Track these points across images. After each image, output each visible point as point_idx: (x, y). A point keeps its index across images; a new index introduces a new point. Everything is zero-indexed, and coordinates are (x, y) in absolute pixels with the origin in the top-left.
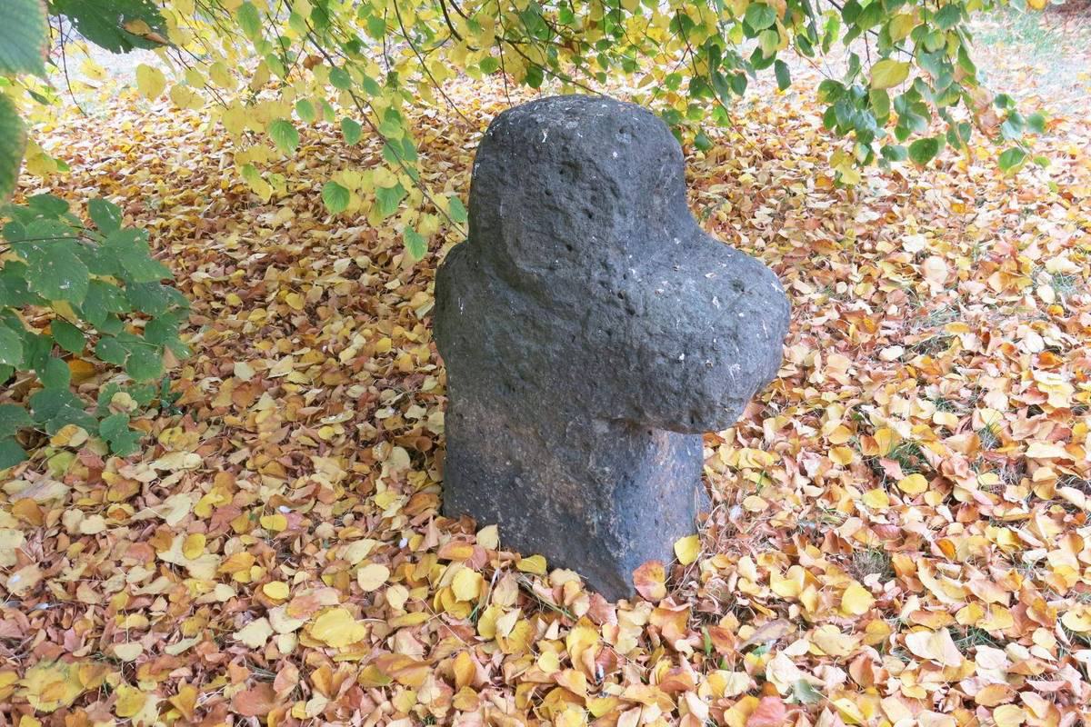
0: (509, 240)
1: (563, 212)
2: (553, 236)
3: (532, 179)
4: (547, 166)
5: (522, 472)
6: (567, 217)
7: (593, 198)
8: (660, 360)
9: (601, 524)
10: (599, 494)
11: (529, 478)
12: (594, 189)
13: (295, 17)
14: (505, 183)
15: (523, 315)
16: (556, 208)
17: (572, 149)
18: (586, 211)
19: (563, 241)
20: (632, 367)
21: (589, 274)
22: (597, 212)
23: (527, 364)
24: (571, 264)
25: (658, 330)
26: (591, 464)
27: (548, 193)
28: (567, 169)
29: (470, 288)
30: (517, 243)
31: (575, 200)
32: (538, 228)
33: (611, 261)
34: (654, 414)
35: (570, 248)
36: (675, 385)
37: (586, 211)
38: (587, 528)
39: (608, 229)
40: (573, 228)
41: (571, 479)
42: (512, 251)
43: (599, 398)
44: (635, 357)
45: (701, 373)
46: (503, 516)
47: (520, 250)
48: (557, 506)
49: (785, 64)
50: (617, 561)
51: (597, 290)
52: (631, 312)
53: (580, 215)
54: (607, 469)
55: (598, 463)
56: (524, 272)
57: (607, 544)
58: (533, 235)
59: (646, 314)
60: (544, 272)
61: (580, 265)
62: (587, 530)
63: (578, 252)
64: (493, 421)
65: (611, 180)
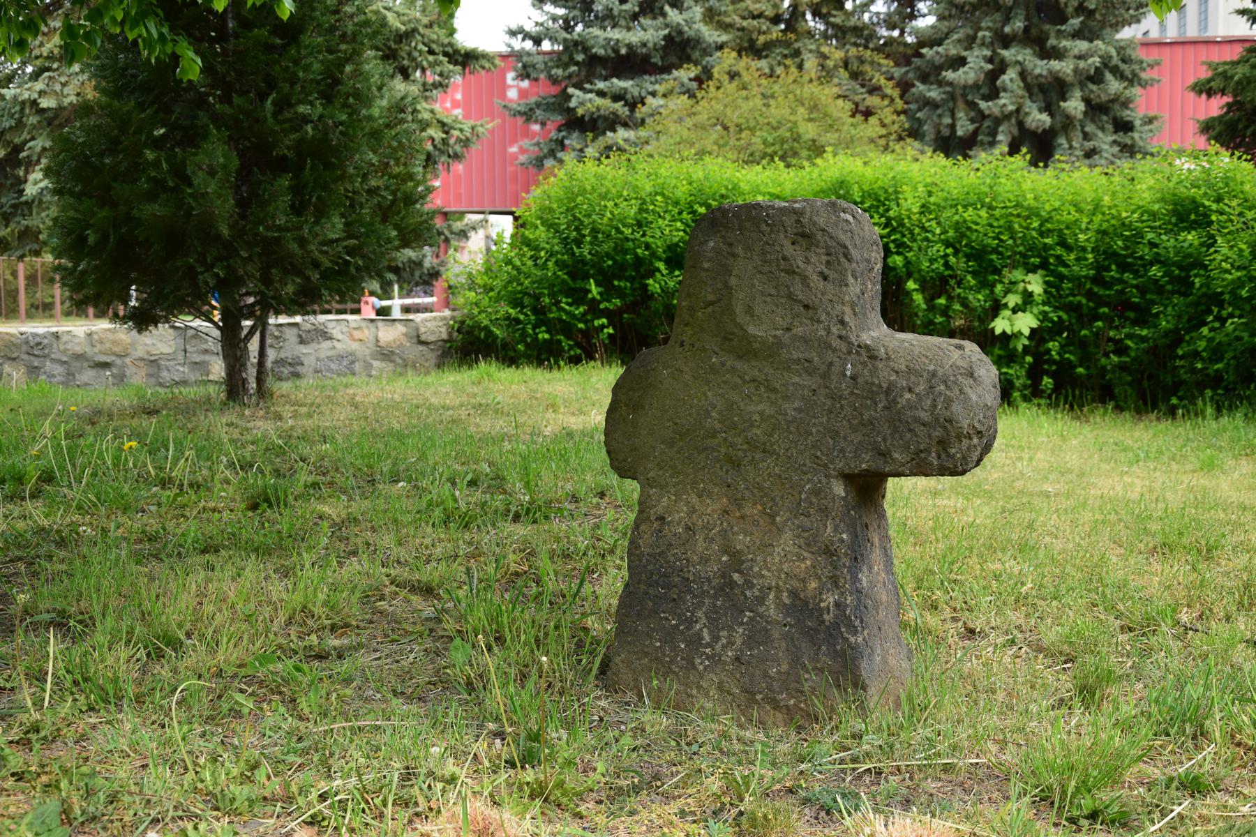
0: (739, 309)
1: (800, 275)
2: (790, 297)
3: (768, 248)
4: (782, 236)
5: (742, 562)
6: (804, 278)
7: (828, 263)
8: (907, 396)
9: (837, 604)
10: (835, 568)
11: (751, 568)
12: (828, 254)
13: (101, 352)
14: (734, 255)
15: (754, 381)
16: (794, 272)
17: (805, 220)
18: (821, 274)
19: (800, 301)
20: (880, 406)
21: (829, 332)
22: (832, 274)
23: (758, 432)
24: (808, 322)
25: (903, 368)
26: (828, 530)
27: (784, 259)
28: (800, 239)
29: (686, 369)
30: (749, 310)
31: (813, 264)
32: (773, 292)
33: (847, 319)
34: (902, 453)
35: (806, 307)
36: (924, 416)
37: (821, 274)
38: (821, 611)
39: (844, 289)
40: (810, 289)
41: (806, 554)
42: (741, 318)
43: (842, 451)
44: (883, 396)
45: (948, 402)
46: (711, 632)
47: (752, 316)
48: (785, 594)
49: (1042, 59)
50: (854, 648)
51: (835, 343)
52: (873, 357)
53: (815, 278)
54: (844, 536)
55: (836, 529)
56: (754, 336)
57: (843, 630)
58: (768, 299)
59: (889, 358)
60: (779, 333)
61: (819, 322)
62: (822, 615)
63: (816, 309)
64: (709, 511)
65: (845, 247)
